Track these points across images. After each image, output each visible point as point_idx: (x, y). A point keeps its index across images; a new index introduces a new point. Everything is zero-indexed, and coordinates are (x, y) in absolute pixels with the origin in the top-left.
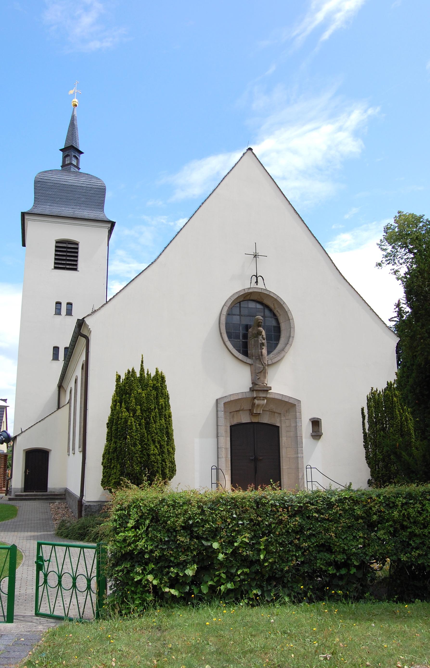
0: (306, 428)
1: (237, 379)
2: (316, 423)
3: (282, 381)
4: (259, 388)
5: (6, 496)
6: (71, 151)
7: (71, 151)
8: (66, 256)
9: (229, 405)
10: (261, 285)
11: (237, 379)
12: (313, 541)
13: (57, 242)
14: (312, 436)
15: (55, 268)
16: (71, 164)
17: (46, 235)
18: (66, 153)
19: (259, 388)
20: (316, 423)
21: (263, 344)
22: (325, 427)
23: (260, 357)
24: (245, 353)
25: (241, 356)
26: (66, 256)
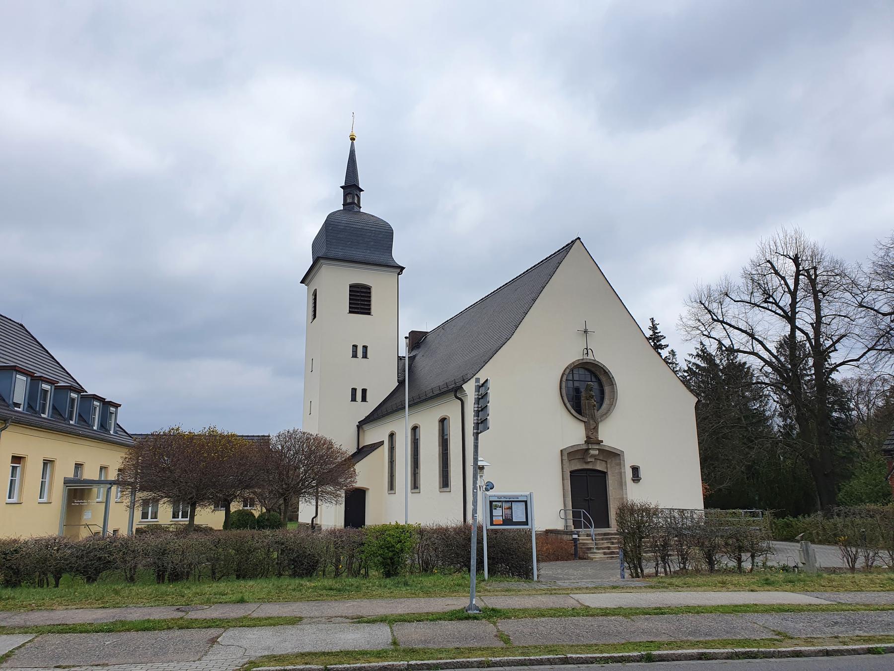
0: (629, 474)
1: (573, 433)
2: (635, 470)
3: (610, 434)
4: (592, 439)
5: (116, 528)
6: (351, 189)
7: (351, 189)
8: (360, 299)
9: (570, 454)
10: (590, 357)
11: (573, 433)
12: (653, 571)
13: (350, 286)
14: (633, 480)
15: (350, 312)
16: (353, 203)
17: (338, 281)
18: (348, 190)
19: (592, 439)
20: (635, 470)
21: (594, 406)
22: (642, 474)
23: (593, 417)
24: (579, 412)
25: (573, 411)
26: (360, 299)
